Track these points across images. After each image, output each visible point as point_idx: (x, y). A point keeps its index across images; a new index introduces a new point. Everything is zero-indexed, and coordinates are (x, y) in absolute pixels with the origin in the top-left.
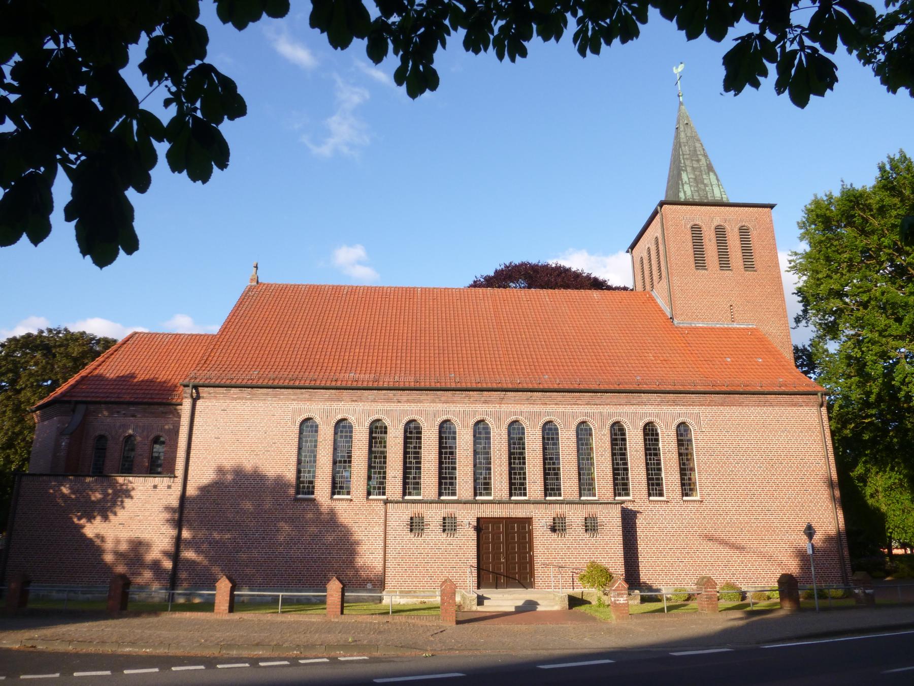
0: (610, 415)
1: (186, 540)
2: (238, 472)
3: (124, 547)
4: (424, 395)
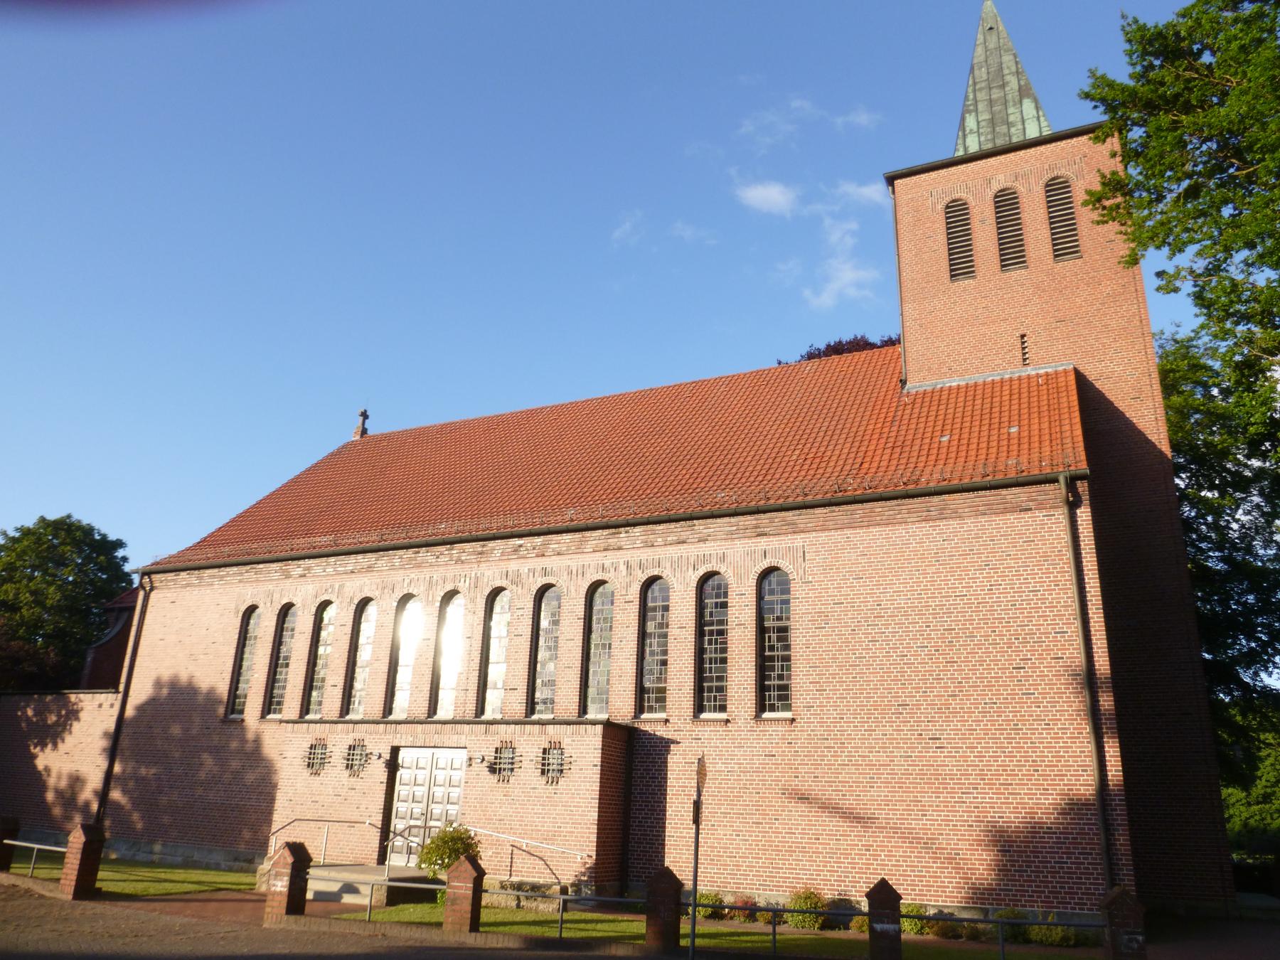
2: (174, 685)
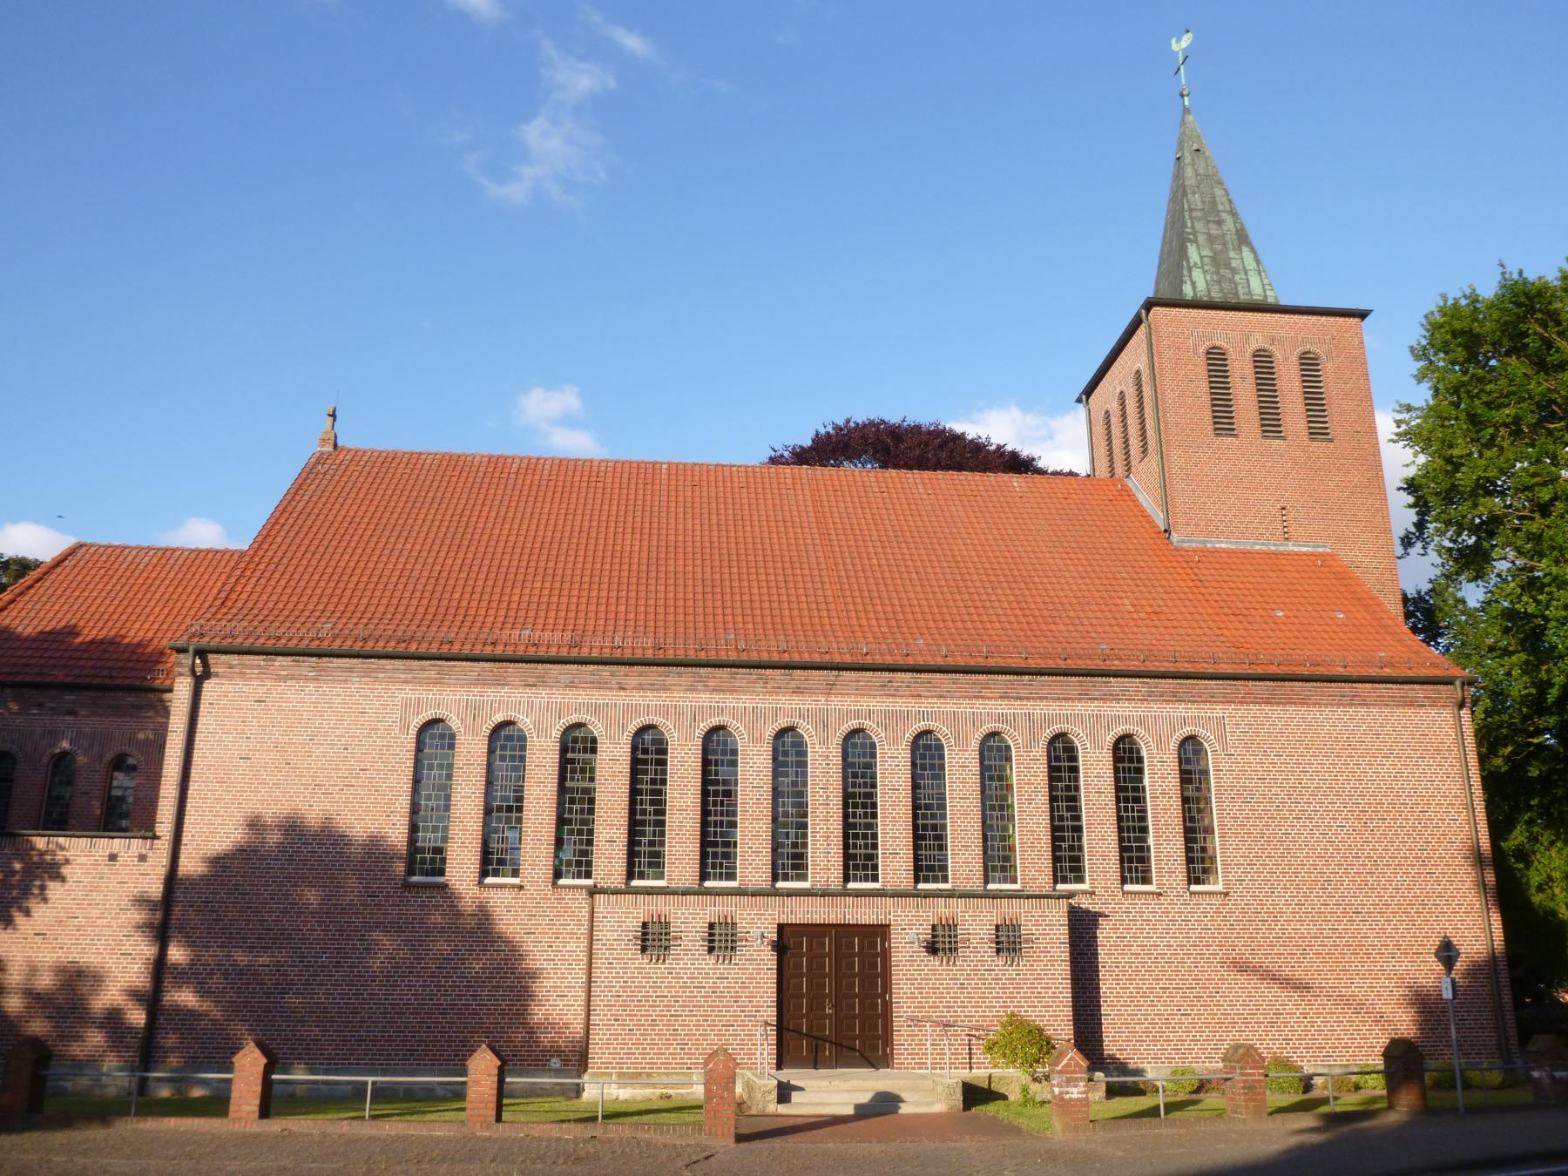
1: (175, 966)
2: (293, 828)
3: (45, 981)
4: (672, 676)
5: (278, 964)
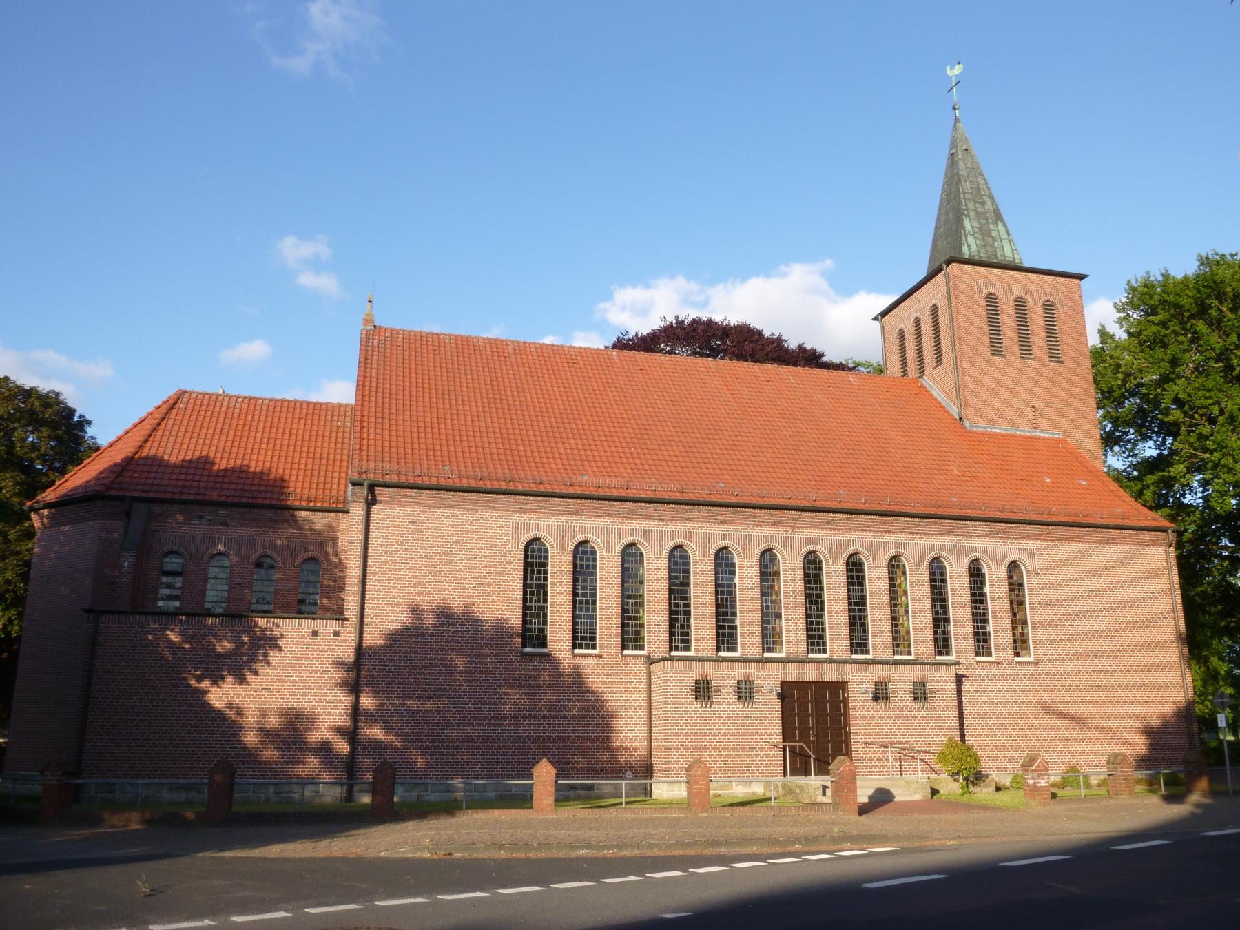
0: (930, 548)
1: (366, 711)
2: (443, 614)
3: (273, 722)
4: (695, 512)
5: (438, 709)
